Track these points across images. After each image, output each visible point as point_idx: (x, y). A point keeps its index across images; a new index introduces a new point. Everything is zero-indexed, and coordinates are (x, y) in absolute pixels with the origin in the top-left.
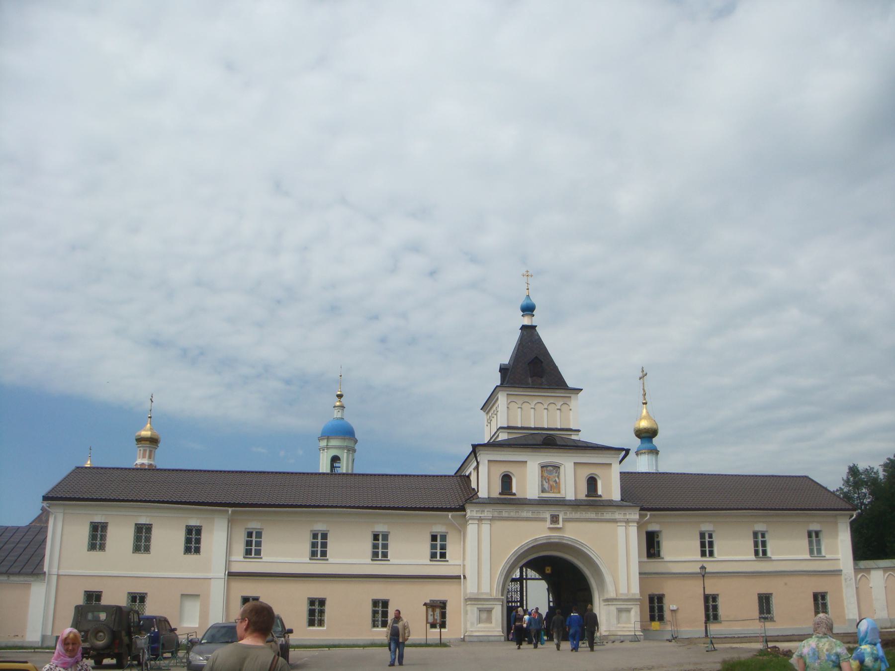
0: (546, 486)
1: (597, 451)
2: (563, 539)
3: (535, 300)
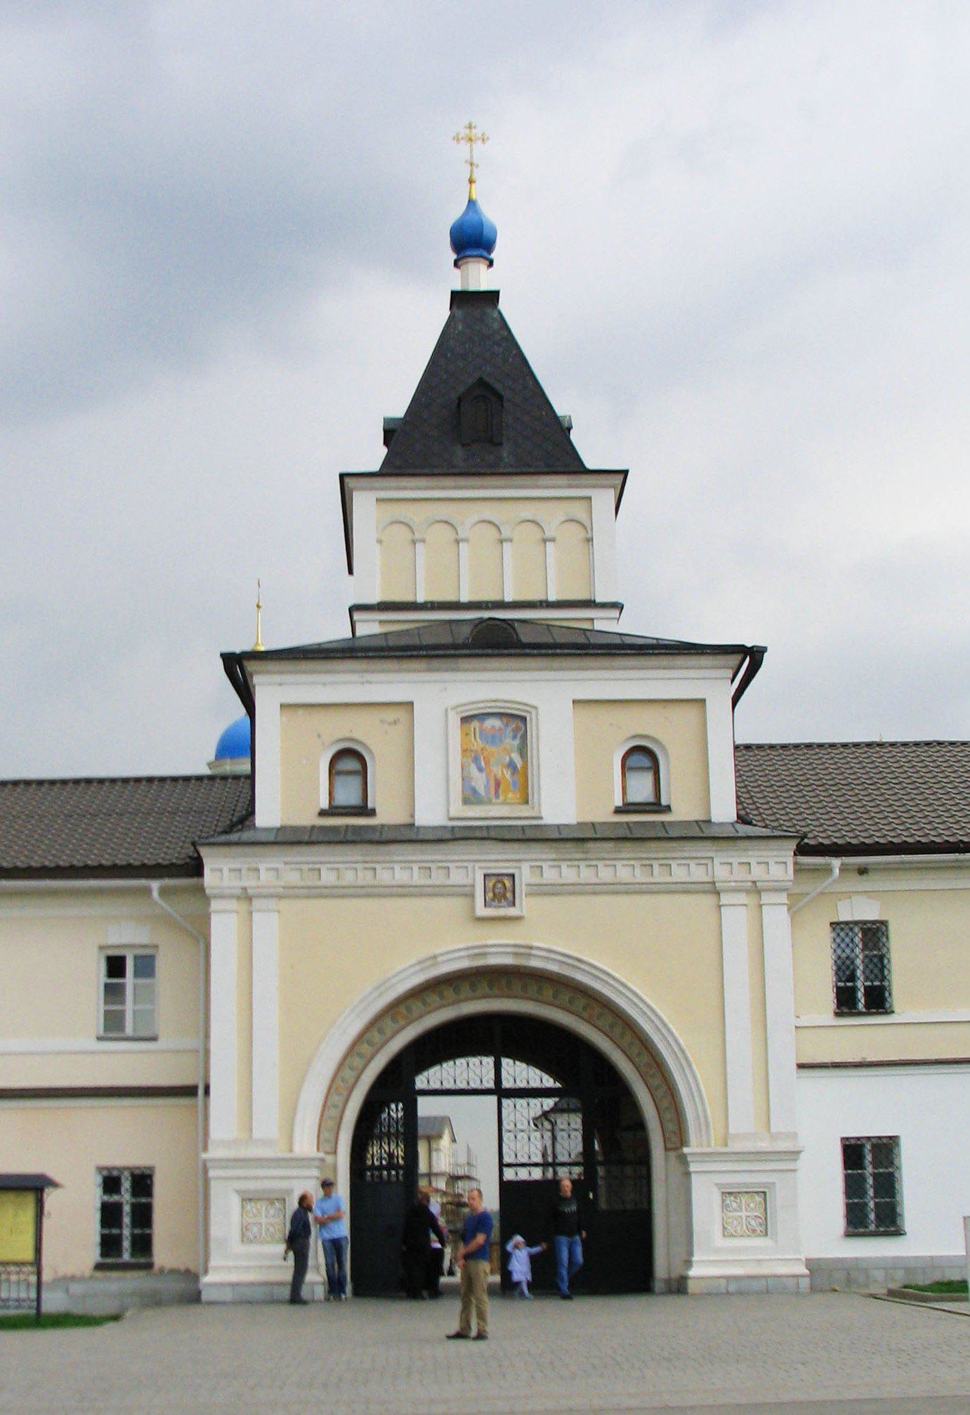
0: (480, 782)
1: (654, 661)
2: (485, 954)
3: (492, 213)
